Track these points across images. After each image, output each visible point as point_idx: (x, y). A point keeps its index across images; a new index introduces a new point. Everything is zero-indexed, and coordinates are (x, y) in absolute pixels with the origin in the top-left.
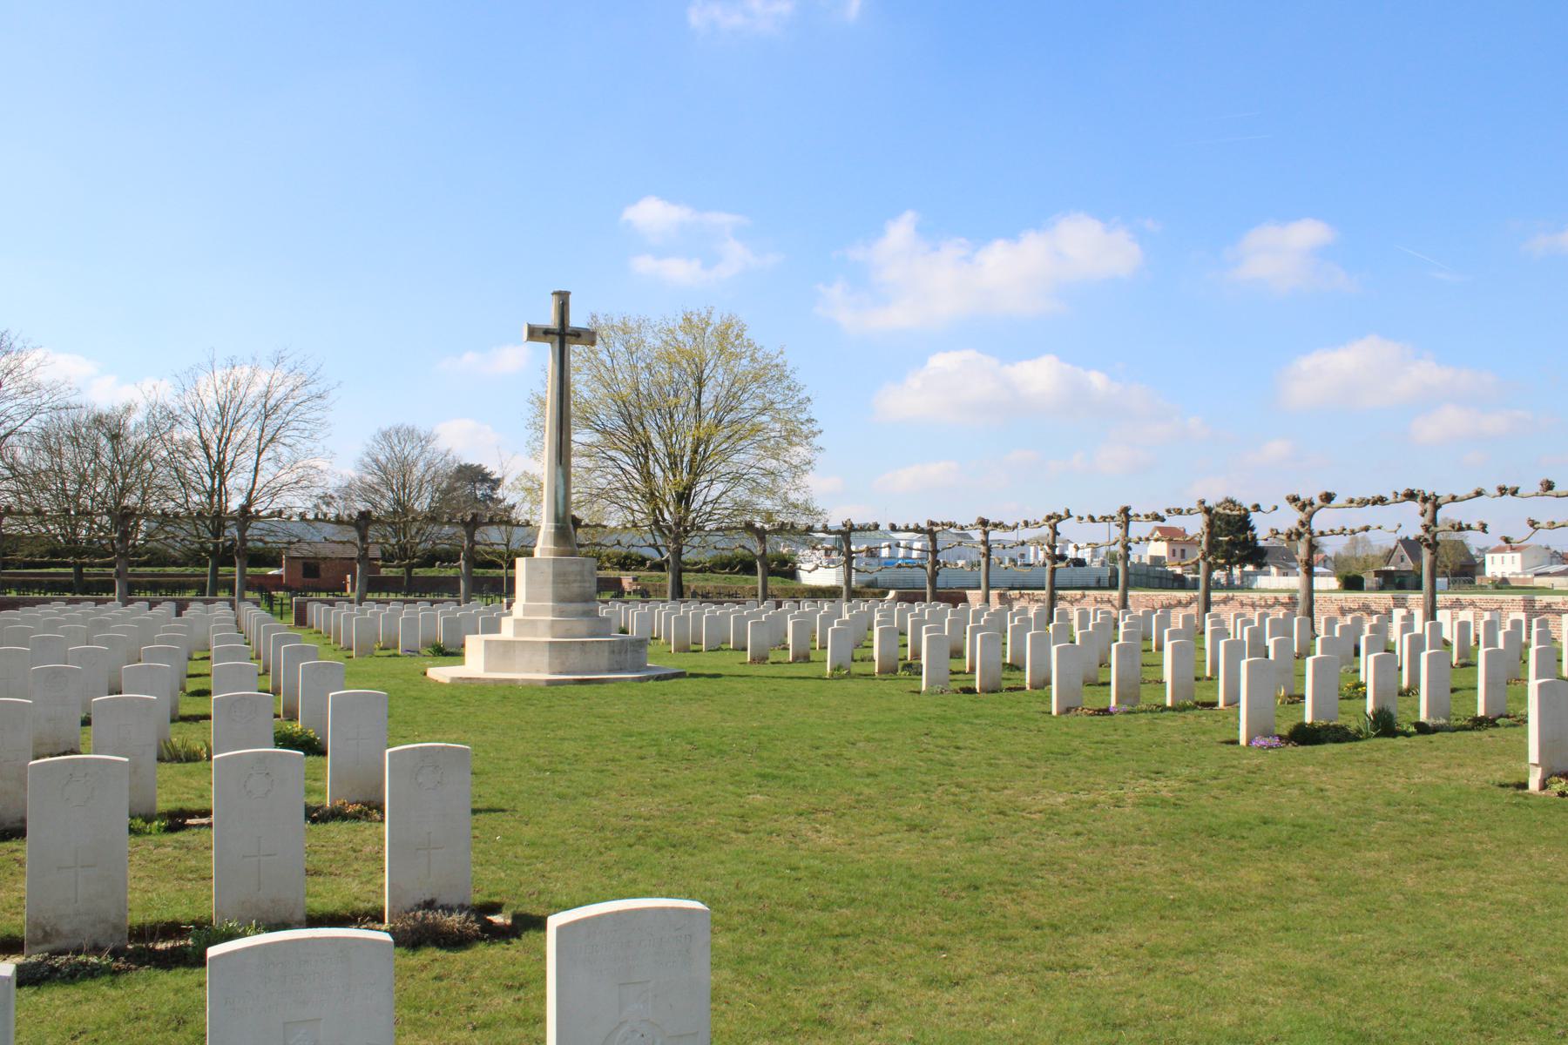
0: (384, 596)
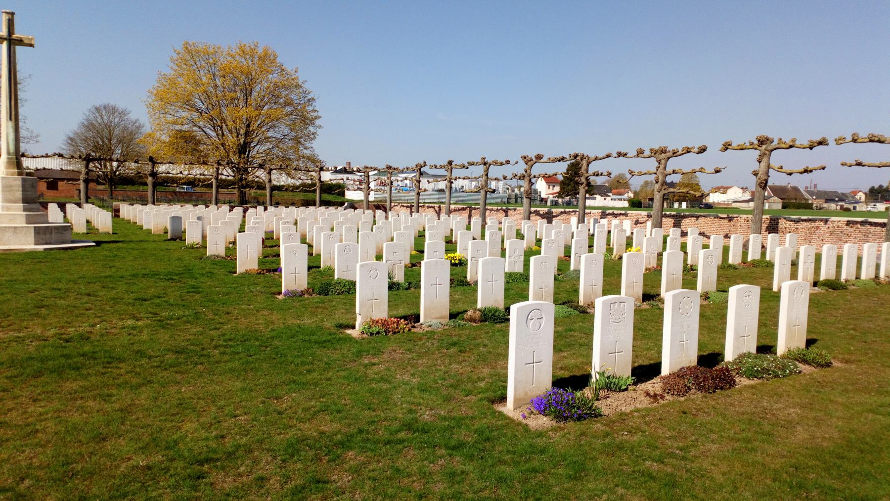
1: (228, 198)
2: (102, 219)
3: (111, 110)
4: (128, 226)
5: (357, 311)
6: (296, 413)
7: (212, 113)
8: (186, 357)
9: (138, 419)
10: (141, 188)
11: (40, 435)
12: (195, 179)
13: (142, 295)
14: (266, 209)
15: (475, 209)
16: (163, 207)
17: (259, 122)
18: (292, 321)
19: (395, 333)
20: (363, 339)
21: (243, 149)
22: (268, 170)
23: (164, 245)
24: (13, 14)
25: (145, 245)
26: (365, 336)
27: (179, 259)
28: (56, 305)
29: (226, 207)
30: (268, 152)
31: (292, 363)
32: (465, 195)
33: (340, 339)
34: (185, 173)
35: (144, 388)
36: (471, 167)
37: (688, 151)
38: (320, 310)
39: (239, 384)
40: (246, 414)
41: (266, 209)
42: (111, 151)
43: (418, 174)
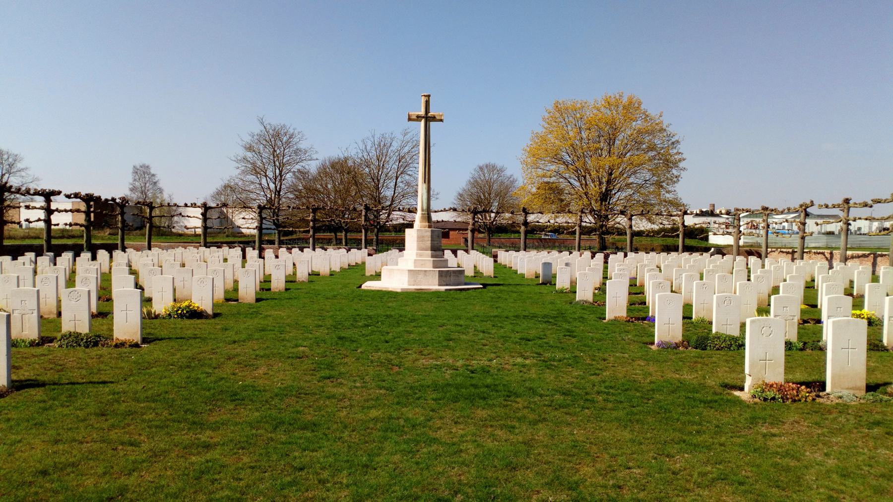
1: (588, 244)
2: (486, 264)
3: (492, 168)
4: (505, 271)
5: (747, 371)
6: (692, 476)
7: (577, 164)
8: (574, 399)
9: (539, 454)
10: (513, 236)
11: (463, 455)
12: (560, 227)
13: (525, 335)
14: (626, 256)
15: (882, 256)
16: (533, 253)
17: (621, 169)
18: (670, 375)
19: (794, 401)
20: (756, 403)
21: (605, 197)
22: (629, 216)
23: (537, 289)
24: (429, 96)
25: (522, 289)
26: (757, 400)
27: (552, 303)
28: (460, 339)
29: (587, 254)
30: (629, 199)
31: (678, 420)
32: (863, 238)
33: (728, 401)
34: (552, 221)
35: (540, 425)
36: (876, 206)
38: (699, 366)
39: (627, 435)
40: (639, 467)
41: (626, 256)
42: (490, 204)
43: (803, 215)
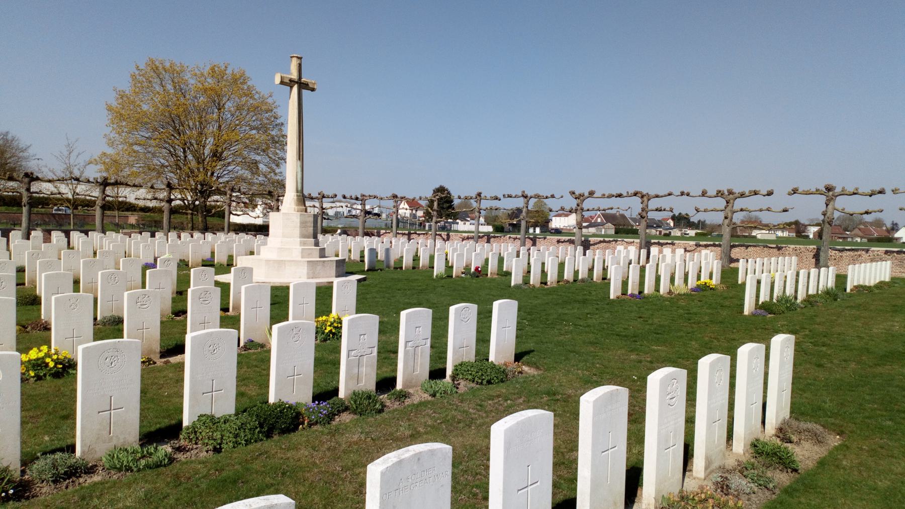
0: (88, 198)
24: (300, 58)
37: (756, 193)
